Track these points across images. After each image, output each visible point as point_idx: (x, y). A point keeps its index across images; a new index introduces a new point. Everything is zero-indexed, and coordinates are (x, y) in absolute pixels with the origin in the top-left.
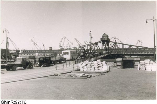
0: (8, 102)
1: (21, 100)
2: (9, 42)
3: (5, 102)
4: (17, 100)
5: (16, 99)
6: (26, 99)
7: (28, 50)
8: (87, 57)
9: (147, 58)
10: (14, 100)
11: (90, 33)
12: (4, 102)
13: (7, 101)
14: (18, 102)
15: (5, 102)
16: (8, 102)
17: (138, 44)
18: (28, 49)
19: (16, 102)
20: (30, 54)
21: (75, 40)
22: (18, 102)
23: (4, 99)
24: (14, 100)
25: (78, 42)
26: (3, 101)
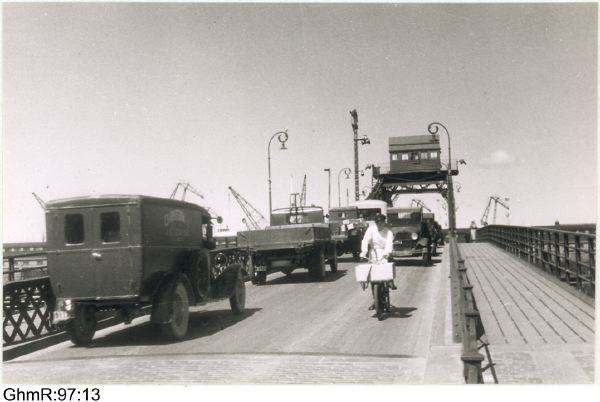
0: (30, 395)
1: (81, 388)
2: (483, 309)
3: (21, 395)
4: (66, 387)
5: (62, 382)
6: (102, 381)
7: (456, 213)
8: (300, 254)
9: (128, 220)
10: (55, 388)
11: (270, 182)
12: (16, 393)
13: (25, 388)
14: (69, 393)
15: (21, 395)
16: (30, 395)
17: (491, 215)
18: (528, 224)
19: (62, 392)
20: (27, 262)
21: (232, 196)
22: (69, 393)
23: (14, 382)
24: (55, 388)
25: (243, 206)
26: (11, 392)
